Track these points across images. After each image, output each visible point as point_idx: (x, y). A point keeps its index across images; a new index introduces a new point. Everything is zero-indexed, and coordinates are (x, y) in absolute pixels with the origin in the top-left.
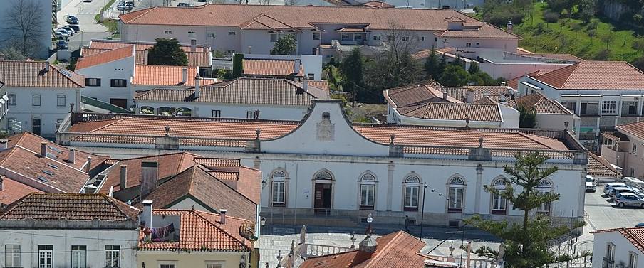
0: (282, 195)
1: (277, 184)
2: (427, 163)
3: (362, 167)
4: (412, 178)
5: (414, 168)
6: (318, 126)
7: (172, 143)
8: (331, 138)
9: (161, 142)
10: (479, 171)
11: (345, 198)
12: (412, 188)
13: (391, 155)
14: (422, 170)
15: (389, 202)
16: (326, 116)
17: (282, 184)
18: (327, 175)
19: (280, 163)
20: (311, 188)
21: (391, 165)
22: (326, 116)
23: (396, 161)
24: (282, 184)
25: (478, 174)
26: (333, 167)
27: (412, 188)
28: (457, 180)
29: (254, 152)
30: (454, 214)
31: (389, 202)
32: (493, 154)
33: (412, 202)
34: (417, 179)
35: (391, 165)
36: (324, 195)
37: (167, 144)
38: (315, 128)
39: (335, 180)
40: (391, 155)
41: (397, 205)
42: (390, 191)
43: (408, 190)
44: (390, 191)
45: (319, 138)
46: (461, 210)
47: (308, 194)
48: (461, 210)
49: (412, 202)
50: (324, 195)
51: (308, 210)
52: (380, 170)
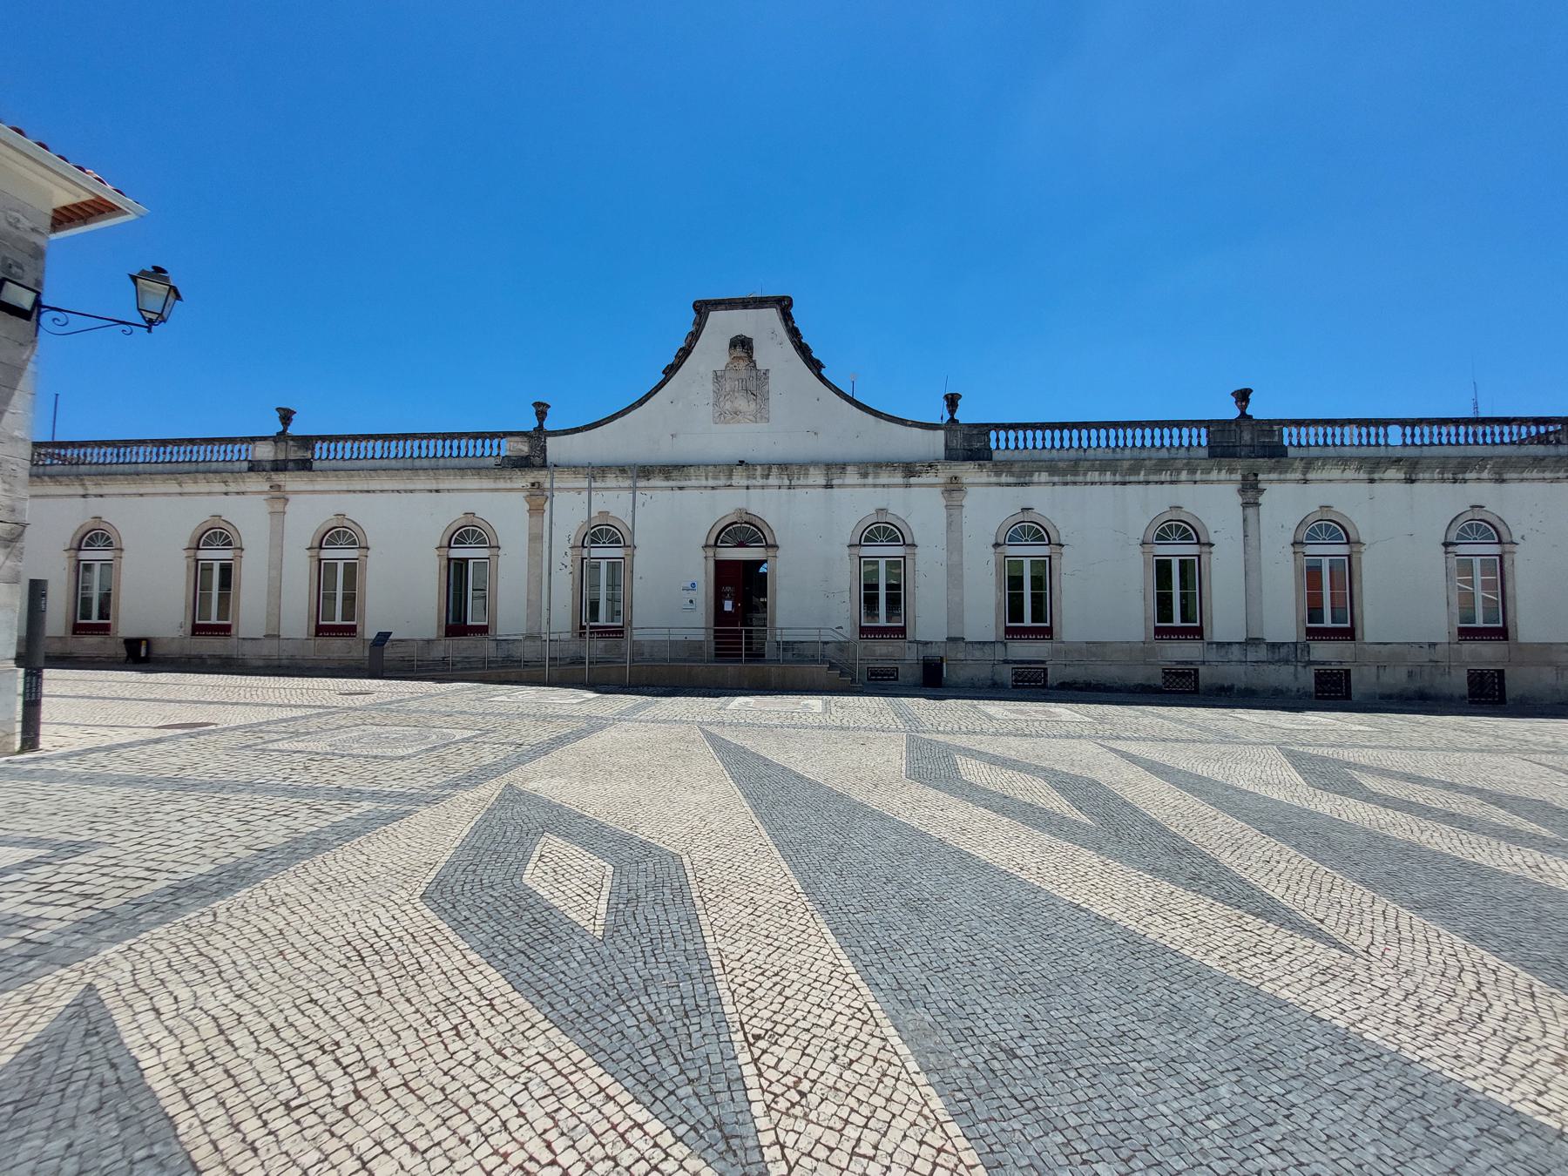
0: (350, 599)
1: (598, 567)
2: (401, 487)
3: (858, 503)
4: (338, 534)
5: (95, 507)
6: (717, 377)
7: (296, 454)
8: (761, 416)
9: (264, 452)
10: (278, 506)
11: (811, 596)
12: (341, 565)
13: (952, 455)
14: (1046, 500)
15: (955, 612)
16: (742, 345)
17: (614, 567)
18: (1178, 529)
19: (613, 501)
20: (700, 573)
21: (954, 487)
22: (742, 345)
23: (969, 473)
24: (614, 567)
25: (1245, 505)
26: (765, 502)
27: (604, 564)
28: (745, 530)
29: (522, 463)
30: (1175, 644)
31: (955, 612)
32: (1288, 436)
33: (1330, 601)
34: (1037, 533)
35: (954, 487)
36: (741, 586)
37: (281, 457)
38: (710, 387)
39: (775, 546)
40: (952, 455)
41: (1282, 619)
42: (955, 574)
43: (331, 567)
44: (955, 574)
45: (721, 417)
46: (903, 630)
47: (692, 595)
48: (353, 629)
49: (1330, 601)
50: (741, 586)
51: (694, 647)
52: (918, 507)
